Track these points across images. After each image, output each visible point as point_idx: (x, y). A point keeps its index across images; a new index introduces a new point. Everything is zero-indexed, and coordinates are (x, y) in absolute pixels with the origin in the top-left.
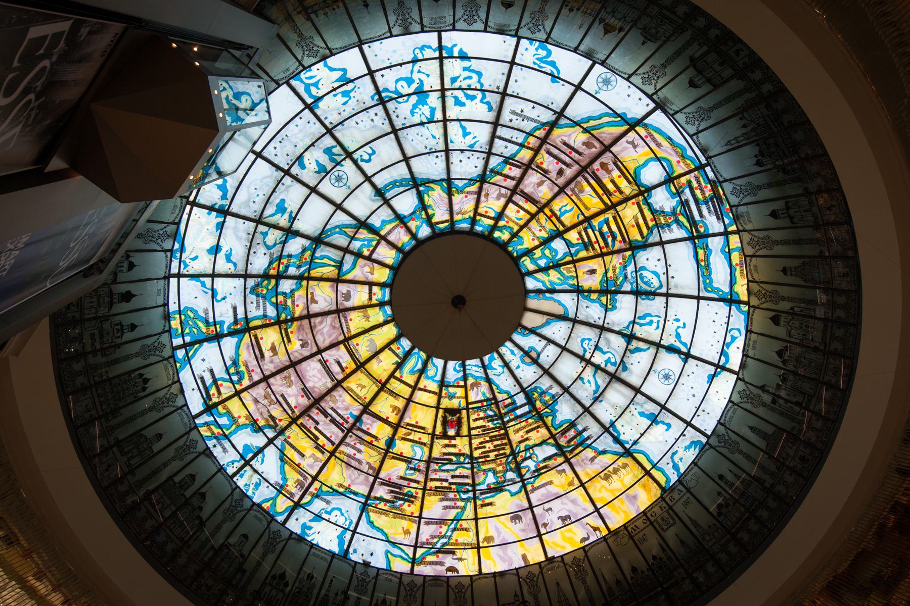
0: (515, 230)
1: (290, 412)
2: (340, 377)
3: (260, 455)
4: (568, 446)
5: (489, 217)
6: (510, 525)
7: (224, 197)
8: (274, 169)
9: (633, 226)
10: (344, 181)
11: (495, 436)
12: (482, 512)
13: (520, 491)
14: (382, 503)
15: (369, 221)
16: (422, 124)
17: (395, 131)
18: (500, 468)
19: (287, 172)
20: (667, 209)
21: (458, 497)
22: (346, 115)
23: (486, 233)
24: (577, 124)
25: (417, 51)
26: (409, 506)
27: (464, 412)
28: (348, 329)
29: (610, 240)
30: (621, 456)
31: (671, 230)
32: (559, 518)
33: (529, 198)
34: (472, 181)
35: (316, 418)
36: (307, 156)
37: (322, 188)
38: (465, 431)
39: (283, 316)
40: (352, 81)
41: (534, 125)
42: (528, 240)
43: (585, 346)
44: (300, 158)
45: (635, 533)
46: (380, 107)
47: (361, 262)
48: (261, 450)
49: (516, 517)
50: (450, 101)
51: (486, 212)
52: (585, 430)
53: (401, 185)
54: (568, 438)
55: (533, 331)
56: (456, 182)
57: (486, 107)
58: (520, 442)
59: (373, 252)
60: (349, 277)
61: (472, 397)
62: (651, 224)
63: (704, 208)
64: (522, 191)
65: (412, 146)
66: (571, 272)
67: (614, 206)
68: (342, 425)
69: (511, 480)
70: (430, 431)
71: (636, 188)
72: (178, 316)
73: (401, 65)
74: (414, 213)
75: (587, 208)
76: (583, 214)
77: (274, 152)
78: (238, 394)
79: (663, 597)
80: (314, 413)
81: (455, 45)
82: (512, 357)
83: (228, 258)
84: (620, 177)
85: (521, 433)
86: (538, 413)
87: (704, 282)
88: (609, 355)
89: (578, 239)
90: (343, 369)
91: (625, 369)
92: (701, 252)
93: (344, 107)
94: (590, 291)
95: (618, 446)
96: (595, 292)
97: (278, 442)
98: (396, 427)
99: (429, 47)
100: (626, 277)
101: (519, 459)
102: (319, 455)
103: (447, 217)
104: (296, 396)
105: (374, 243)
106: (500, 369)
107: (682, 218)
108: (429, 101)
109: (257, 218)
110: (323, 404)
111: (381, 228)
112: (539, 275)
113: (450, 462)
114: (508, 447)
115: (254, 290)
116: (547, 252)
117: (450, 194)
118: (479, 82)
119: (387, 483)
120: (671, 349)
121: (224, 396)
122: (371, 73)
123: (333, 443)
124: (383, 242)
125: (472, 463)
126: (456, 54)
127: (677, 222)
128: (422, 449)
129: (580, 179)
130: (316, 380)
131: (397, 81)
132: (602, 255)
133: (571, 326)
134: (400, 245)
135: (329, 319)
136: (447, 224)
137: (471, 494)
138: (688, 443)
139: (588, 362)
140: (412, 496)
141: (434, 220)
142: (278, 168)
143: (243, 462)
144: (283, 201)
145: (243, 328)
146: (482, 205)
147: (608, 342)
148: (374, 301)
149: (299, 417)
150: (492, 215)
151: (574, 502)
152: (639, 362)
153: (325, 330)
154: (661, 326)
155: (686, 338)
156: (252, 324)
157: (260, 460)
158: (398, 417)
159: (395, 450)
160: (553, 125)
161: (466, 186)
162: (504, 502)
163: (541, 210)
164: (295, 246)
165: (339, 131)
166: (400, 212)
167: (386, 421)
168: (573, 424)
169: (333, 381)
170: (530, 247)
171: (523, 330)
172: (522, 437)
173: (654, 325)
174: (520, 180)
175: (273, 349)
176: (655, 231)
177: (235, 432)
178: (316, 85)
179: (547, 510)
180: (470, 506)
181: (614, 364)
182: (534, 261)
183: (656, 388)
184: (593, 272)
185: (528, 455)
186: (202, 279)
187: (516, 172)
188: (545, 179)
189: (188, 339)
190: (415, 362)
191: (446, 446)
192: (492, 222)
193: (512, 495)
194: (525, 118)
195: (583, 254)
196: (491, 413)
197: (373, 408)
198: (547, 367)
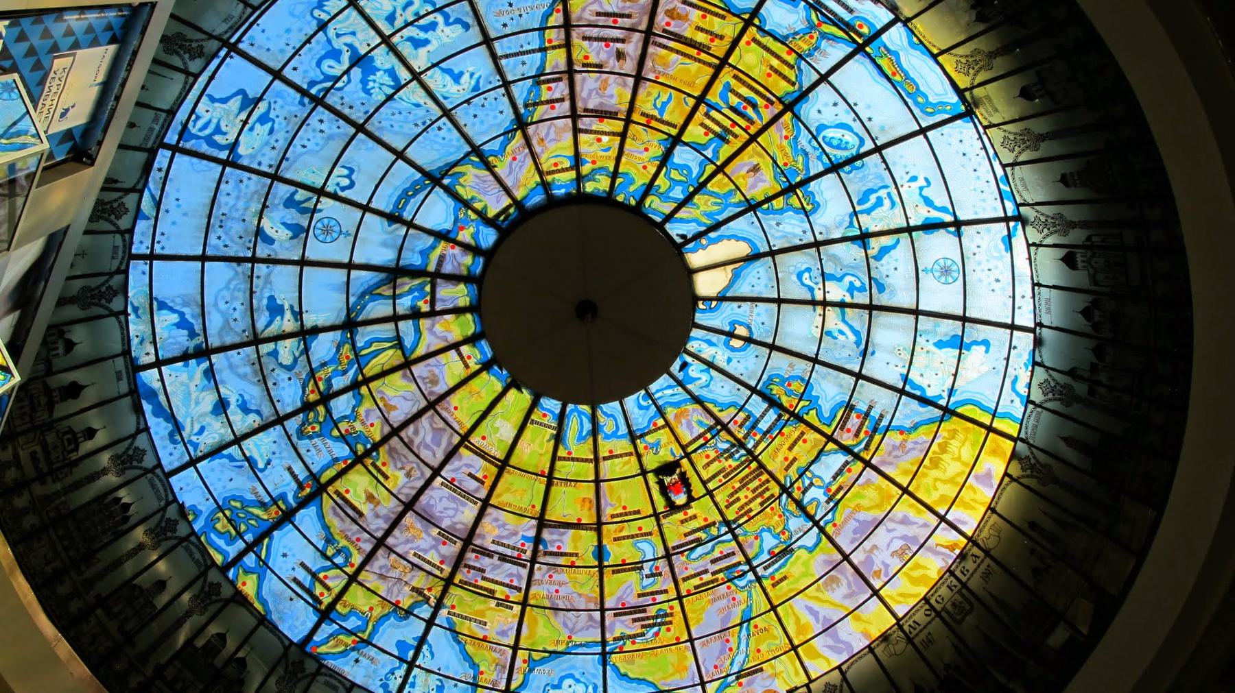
0: (611, 169)
1: (437, 573)
2: (483, 494)
3: (425, 647)
4: (857, 440)
5: (564, 170)
7: (192, 335)
8: (234, 264)
10: (337, 229)
11: (747, 476)
12: (776, 595)
13: (819, 541)
14: (628, 642)
15: (402, 263)
16: (390, 98)
17: (360, 128)
19: (254, 260)
22: (282, 144)
25: (317, 13)
26: (668, 630)
27: (685, 462)
28: (459, 423)
29: (750, 111)
30: (942, 421)
31: (824, 54)
32: (892, 555)
34: (508, 134)
36: (266, 224)
37: (311, 255)
38: (698, 489)
39: (360, 449)
42: (638, 168)
43: (808, 282)
44: (259, 231)
46: (320, 109)
47: (424, 323)
48: (422, 640)
49: (828, 576)
50: (406, 49)
51: (556, 164)
53: (416, 192)
54: (854, 430)
56: (486, 147)
59: (433, 302)
60: (420, 351)
62: (791, 59)
67: (724, 61)
68: (519, 558)
71: (736, 20)
72: (220, 515)
73: (308, 41)
74: (456, 220)
77: (220, 243)
78: (353, 578)
80: (470, 556)
82: (712, 350)
83: (245, 410)
85: (780, 458)
86: (792, 414)
87: (917, 104)
88: (848, 279)
89: (706, 134)
91: (881, 288)
92: (883, 62)
93: (274, 137)
94: (768, 200)
98: (598, 526)
103: (680, 121)
104: (434, 547)
105: (428, 288)
106: (704, 377)
108: (378, 63)
109: (251, 338)
110: (477, 542)
113: (699, 542)
114: (772, 484)
115: (301, 433)
116: (674, 175)
117: (489, 168)
121: (337, 590)
123: (518, 589)
124: (439, 280)
125: (731, 531)
127: (824, 36)
129: (651, 49)
131: (319, 64)
132: (753, 138)
134: (465, 273)
135: (424, 421)
137: (750, 576)
139: (825, 304)
140: (666, 615)
141: (491, 213)
142: (239, 260)
143: (405, 666)
144: (272, 298)
145: (315, 489)
146: (543, 159)
147: (835, 259)
148: (474, 367)
149: (453, 574)
150: (567, 164)
151: (905, 521)
152: (895, 269)
153: (428, 440)
154: (897, 199)
155: (941, 200)
157: (427, 654)
162: (806, 564)
163: (628, 121)
164: (323, 347)
165: (287, 169)
166: (438, 228)
169: (475, 503)
170: (647, 181)
173: (887, 202)
175: (370, 498)
178: (218, 130)
179: (871, 551)
182: (664, 197)
184: (755, 169)
185: (807, 482)
186: (225, 452)
189: (249, 537)
193: (811, 550)
195: (726, 151)
197: (551, 515)
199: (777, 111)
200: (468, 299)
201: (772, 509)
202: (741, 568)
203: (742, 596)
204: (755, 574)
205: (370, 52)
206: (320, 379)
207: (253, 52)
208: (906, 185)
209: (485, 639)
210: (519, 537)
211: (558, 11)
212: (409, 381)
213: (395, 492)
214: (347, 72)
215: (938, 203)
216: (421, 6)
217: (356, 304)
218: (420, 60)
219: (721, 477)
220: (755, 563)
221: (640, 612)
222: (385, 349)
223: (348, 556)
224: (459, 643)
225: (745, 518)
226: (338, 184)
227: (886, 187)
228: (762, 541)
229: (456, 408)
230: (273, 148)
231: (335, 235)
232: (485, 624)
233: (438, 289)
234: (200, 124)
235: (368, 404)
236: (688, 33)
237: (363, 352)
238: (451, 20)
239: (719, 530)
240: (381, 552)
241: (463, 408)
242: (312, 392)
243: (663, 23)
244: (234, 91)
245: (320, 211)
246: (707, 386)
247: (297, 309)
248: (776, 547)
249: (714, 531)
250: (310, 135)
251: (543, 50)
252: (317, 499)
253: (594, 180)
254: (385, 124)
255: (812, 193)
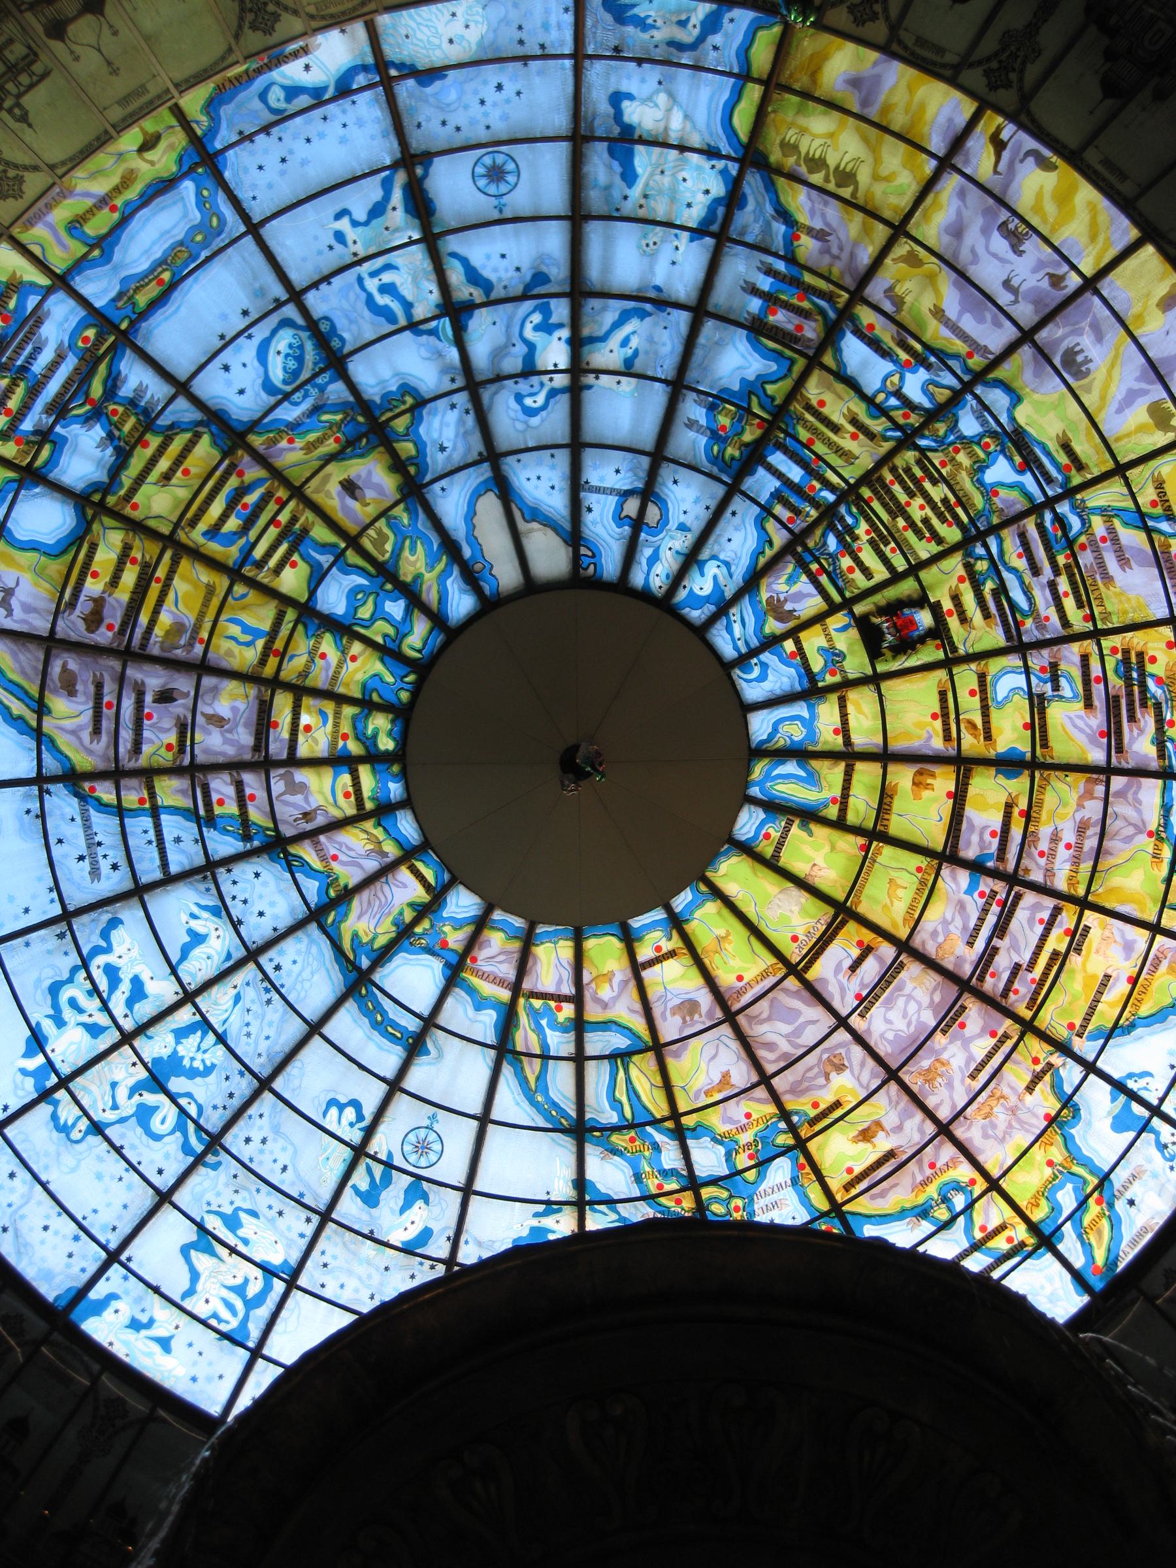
1: (1009, 1044)
2: (888, 951)
3: (1131, 1084)
6: (1099, 373)
9: (186, 472)
10: (422, 1133)
11: (884, 505)
12: (1097, 463)
16: (221, 1039)
18: (962, 457)
20: (98, 432)
21: (1083, 539)
22: (277, 1201)
23: (395, 768)
24: (39, 735)
25: (76, 1135)
26: (1153, 660)
27: (859, 609)
28: (764, 975)
29: (251, 499)
31: (140, 391)
32: (1020, 253)
33: (264, 723)
34: (292, 865)
35: (1005, 976)
36: (397, 1238)
37: (458, 1176)
38: (907, 587)
39: (785, 1139)
40: (200, 1226)
41: (96, 817)
42: (362, 669)
43: (541, 399)
44: (407, 1250)
46: (228, 1140)
47: (593, 1013)
48: (1119, 1086)
49: (1071, 368)
50: (145, 1010)
51: (347, 795)
52: (754, 291)
54: (797, 320)
55: (574, 537)
57: (116, 935)
58: (871, 436)
59: (560, 998)
60: (639, 1025)
61: (813, 604)
62: (155, 441)
63: (39, 366)
64: (256, 748)
65: (279, 1032)
66: (380, 532)
67: (169, 540)
69: (979, 417)
70: (941, 674)
71: (96, 527)
73: (118, 1150)
75: (210, 590)
76: (229, 591)
80: (992, 985)
81: (24, 1072)
84: (95, 575)
85: (847, 443)
88: (529, 333)
89: (294, 565)
90: (867, 950)
91: (540, 278)
92: (142, 300)
93: (262, 1208)
94: (398, 465)
95: (747, 189)
96: (393, 454)
97: (1086, 1048)
99: (54, 1117)
100: (316, 410)
101: (915, 420)
102: (1094, 935)
103: (404, 874)
104: (966, 1043)
105: (537, 1003)
106: (711, 569)
107: (97, 389)
108: (165, 1053)
111: (496, 1004)
112: (431, 596)
113: (1001, 590)
114: (899, 461)
116: (365, 613)
118: (70, 980)
119: (1113, 735)
120: (420, 204)
121: (1008, 1212)
122: (164, 1198)
123: (1057, 911)
125: (982, 536)
126: (40, 1059)
127: (111, 391)
128: (997, 678)
129: (155, 651)
130: (912, 1007)
131: (157, 1138)
133: (511, 460)
136: (420, 866)
137: (1063, 508)
138: (630, 29)
139: (578, 369)
140: (1126, 660)
143: (1156, 1122)
146: (336, 813)
147: (498, 353)
148: (676, 942)
150: (346, 779)
153: (786, 1028)
154: (379, 262)
155: (371, 190)
156: (824, 1206)
157: (1142, 1083)
158: (938, 770)
159: (1024, 747)
160: (72, 778)
161: (311, 872)
162: (1045, 414)
163: (275, 683)
166: (440, 982)
167: (959, 797)
168: (757, 329)
169: (902, 966)
170: (376, 655)
171: (585, 561)
172: (854, 437)
173: (387, 277)
174: (234, 766)
175: (866, 1135)
176: (163, 421)
177: (1087, 1163)
178: (240, 1290)
179: (1014, 291)
180: (1097, 498)
181: (546, 312)
183: (543, 177)
184: (350, 487)
185: (893, 401)
187: (221, 786)
188: (200, 719)
190: (787, 783)
191: (964, 620)
192: (365, 772)
194: (93, 844)
195: (320, 532)
196: (832, 542)
198: (645, 461)
199: (247, 458)
200: (562, 943)
201: (943, 464)
202: (1048, 524)
203: (1098, 525)
204: (1058, 498)
205: (145, 1065)
206: (660, 1186)
207: (126, 1229)
208: (353, 248)
209: (1134, 981)
210: (967, 898)
211: (93, 789)
212: (685, 1048)
213: (864, 1094)
214: (173, 1098)
215: (377, 194)
216: (79, 987)
217: (547, 1116)
218: (162, 990)
219: (887, 550)
220: (1040, 498)
221: (1118, 707)
222: (628, 1080)
223: (958, 1187)
224: (1132, 1026)
225: (959, 511)
226: (352, 1125)
227: (360, 280)
228: (1002, 484)
229: (740, 978)
230: (280, 1213)
231: (432, 1137)
232: (1107, 977)
233: (541, 988)
234: (225, 1314)
235: (714, 1119)
236: (123, 594)
237: (628, 1114)
238: (104, 944)
239: (980, 558)
240: (959, 1132)
241: (740, 964)
242: (678, 1202)
243: (110, 634)
244: (182, 1260)
245: (390, 1155)
246: (727, 564)
247: (541, 1208)
248: (1010, 459)
249: (982, 566)
250: (267, 1158)
251: (155, 812)
252: (849, 1217)
253: (375, 736)
254: (263, 1046)
255: (384, 396)
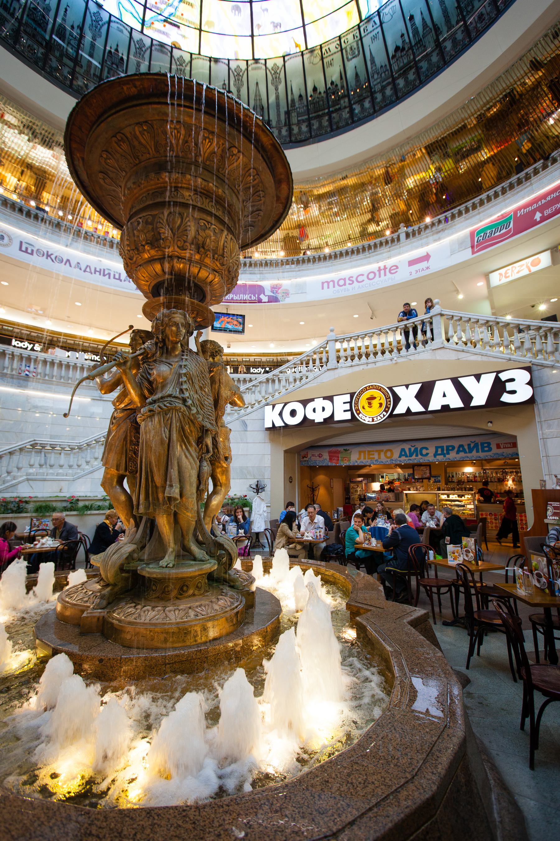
45: (326, 55)
79: (327, 118)
